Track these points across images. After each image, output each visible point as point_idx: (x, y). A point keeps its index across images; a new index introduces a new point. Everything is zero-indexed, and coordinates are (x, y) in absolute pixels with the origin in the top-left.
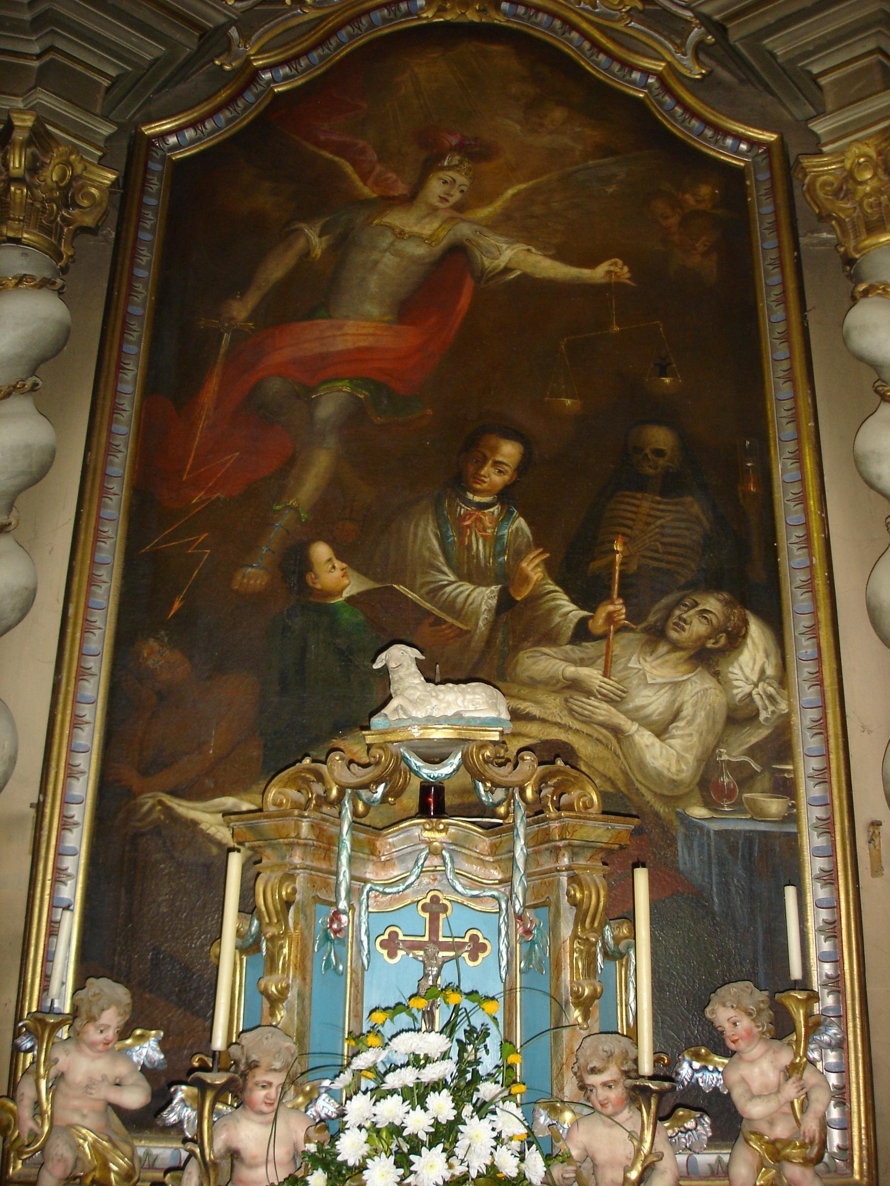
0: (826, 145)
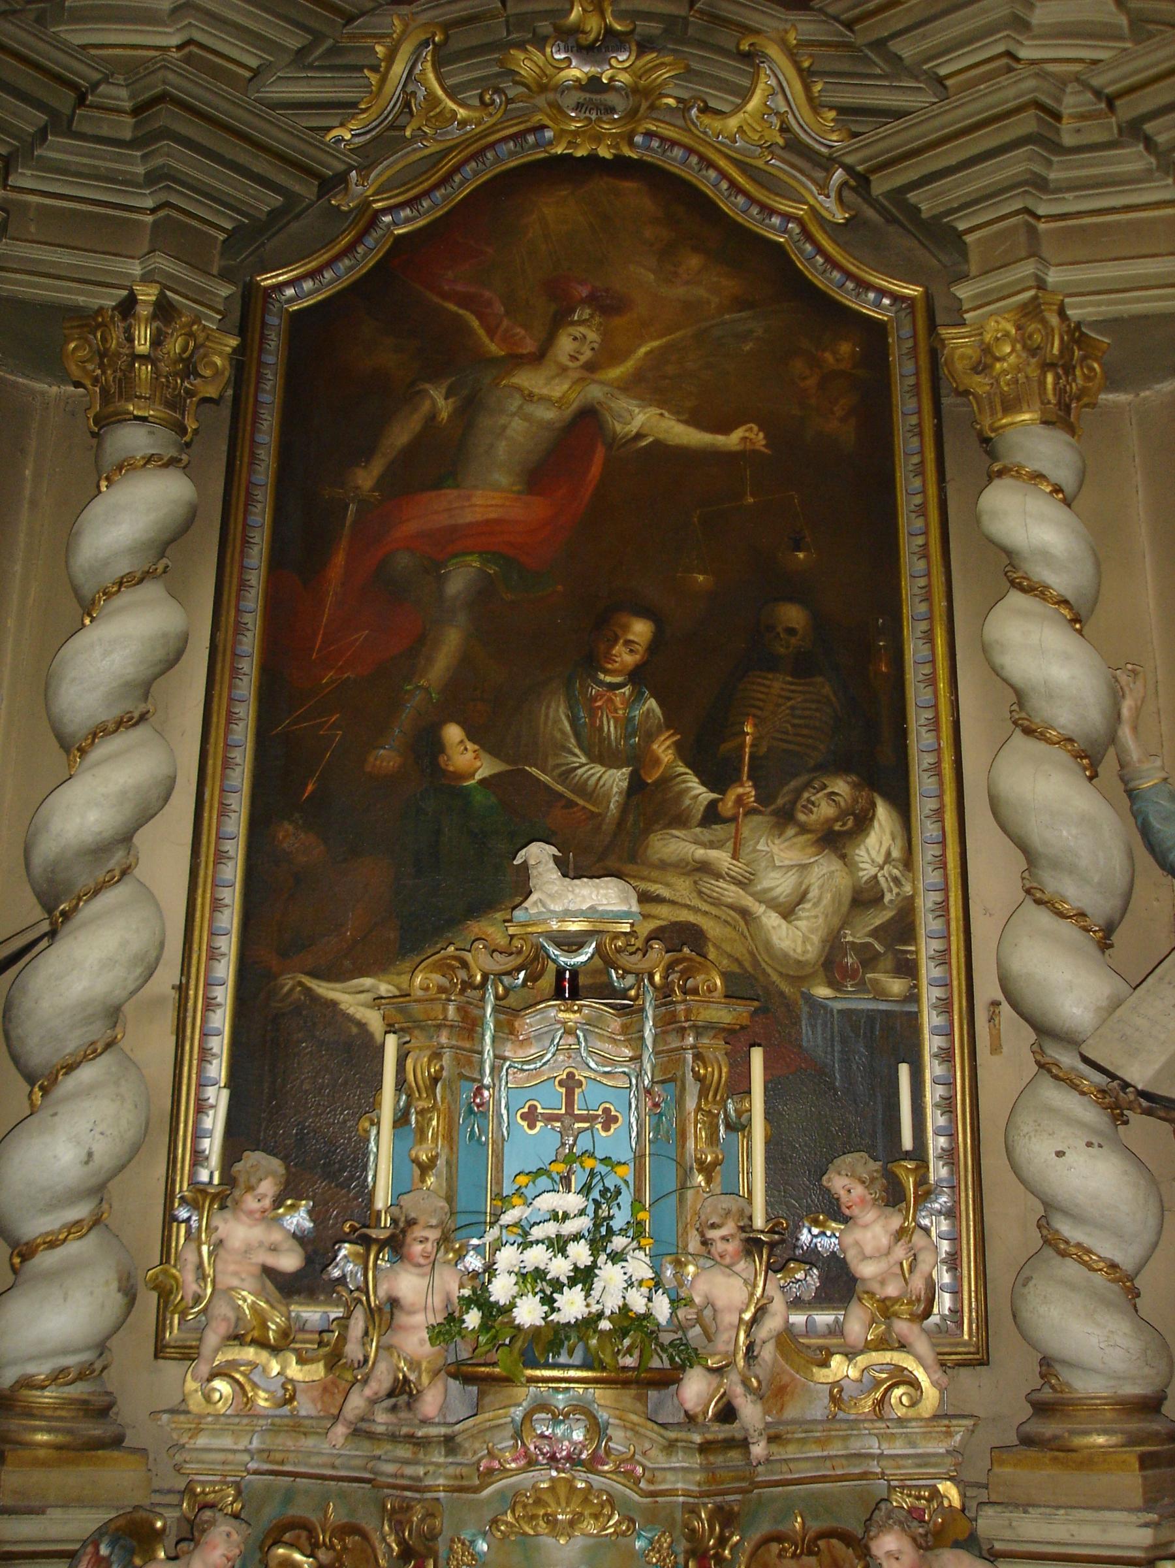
0: (967, 311)
